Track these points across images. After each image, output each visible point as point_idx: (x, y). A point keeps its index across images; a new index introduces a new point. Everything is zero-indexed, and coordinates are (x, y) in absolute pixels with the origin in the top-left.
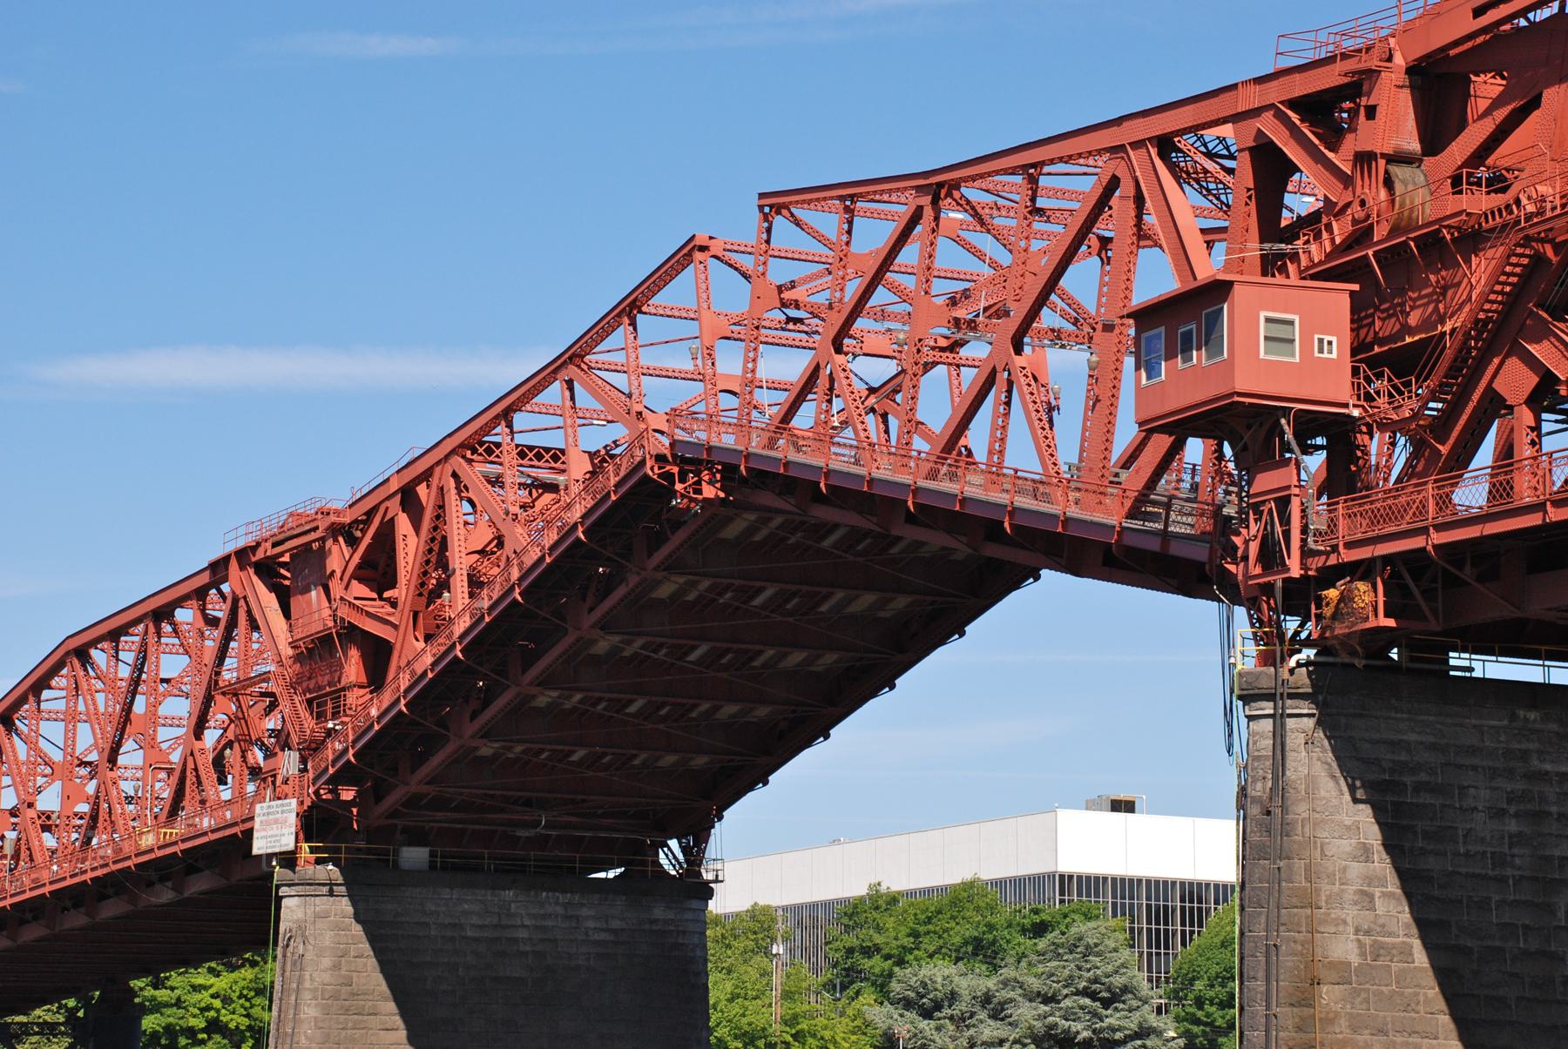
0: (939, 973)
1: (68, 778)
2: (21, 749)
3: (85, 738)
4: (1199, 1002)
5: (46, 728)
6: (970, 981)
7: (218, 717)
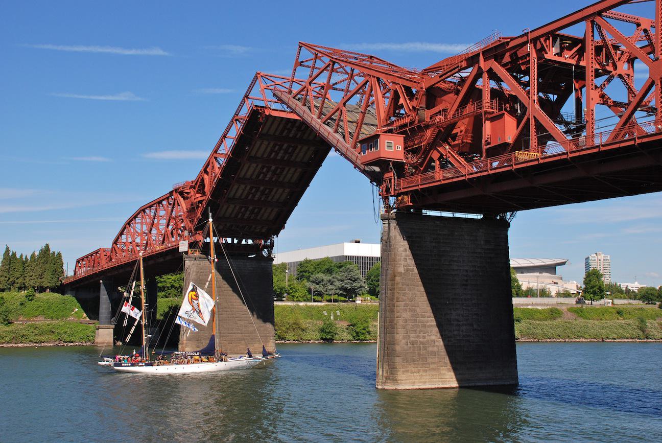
0: (320, 276)
1: (142, 236)
2: (132, 230)
3: (145, 228)
4: (372, 281)
5: (137, 225)
6: (326, 277)
7: (172, 224)
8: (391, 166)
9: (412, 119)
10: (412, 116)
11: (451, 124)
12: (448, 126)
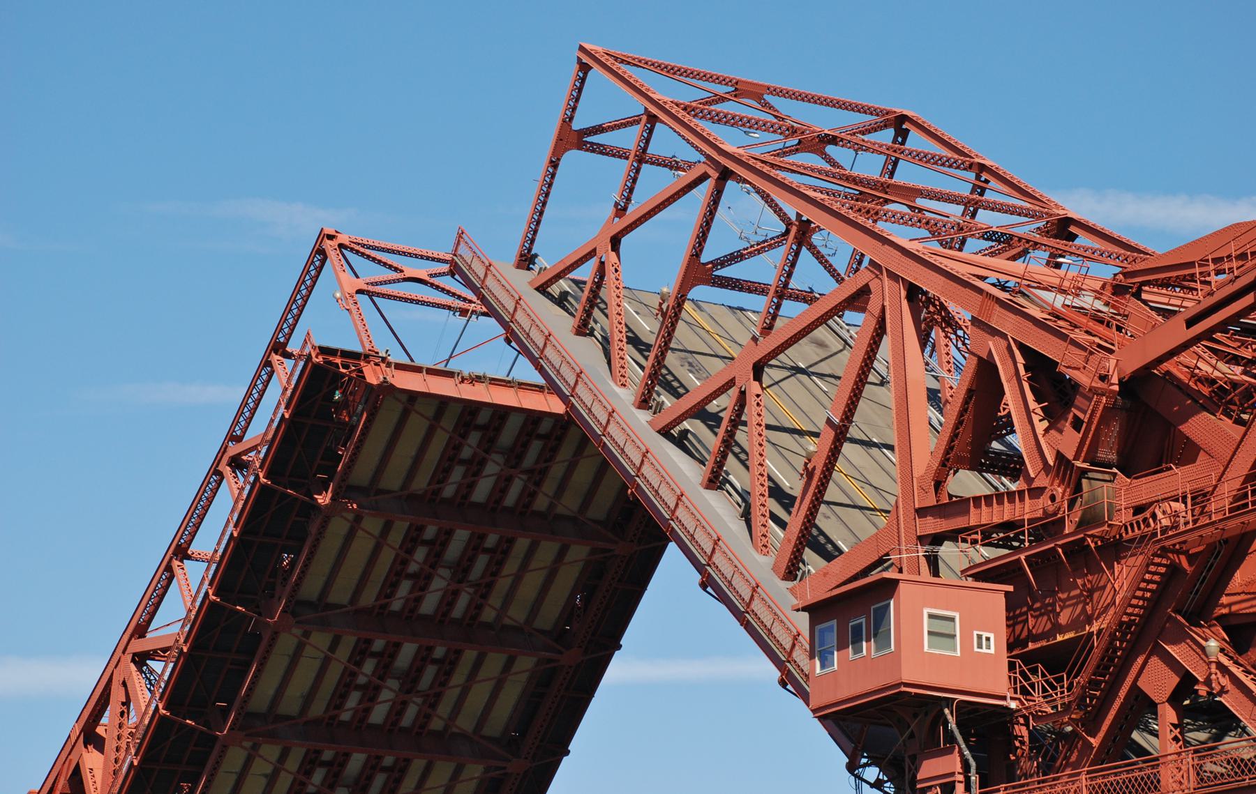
8: (952, 725)
9: (1051, 509)
10: (1053, 498)
11: (1226, 541)
12: (1212, 549)
